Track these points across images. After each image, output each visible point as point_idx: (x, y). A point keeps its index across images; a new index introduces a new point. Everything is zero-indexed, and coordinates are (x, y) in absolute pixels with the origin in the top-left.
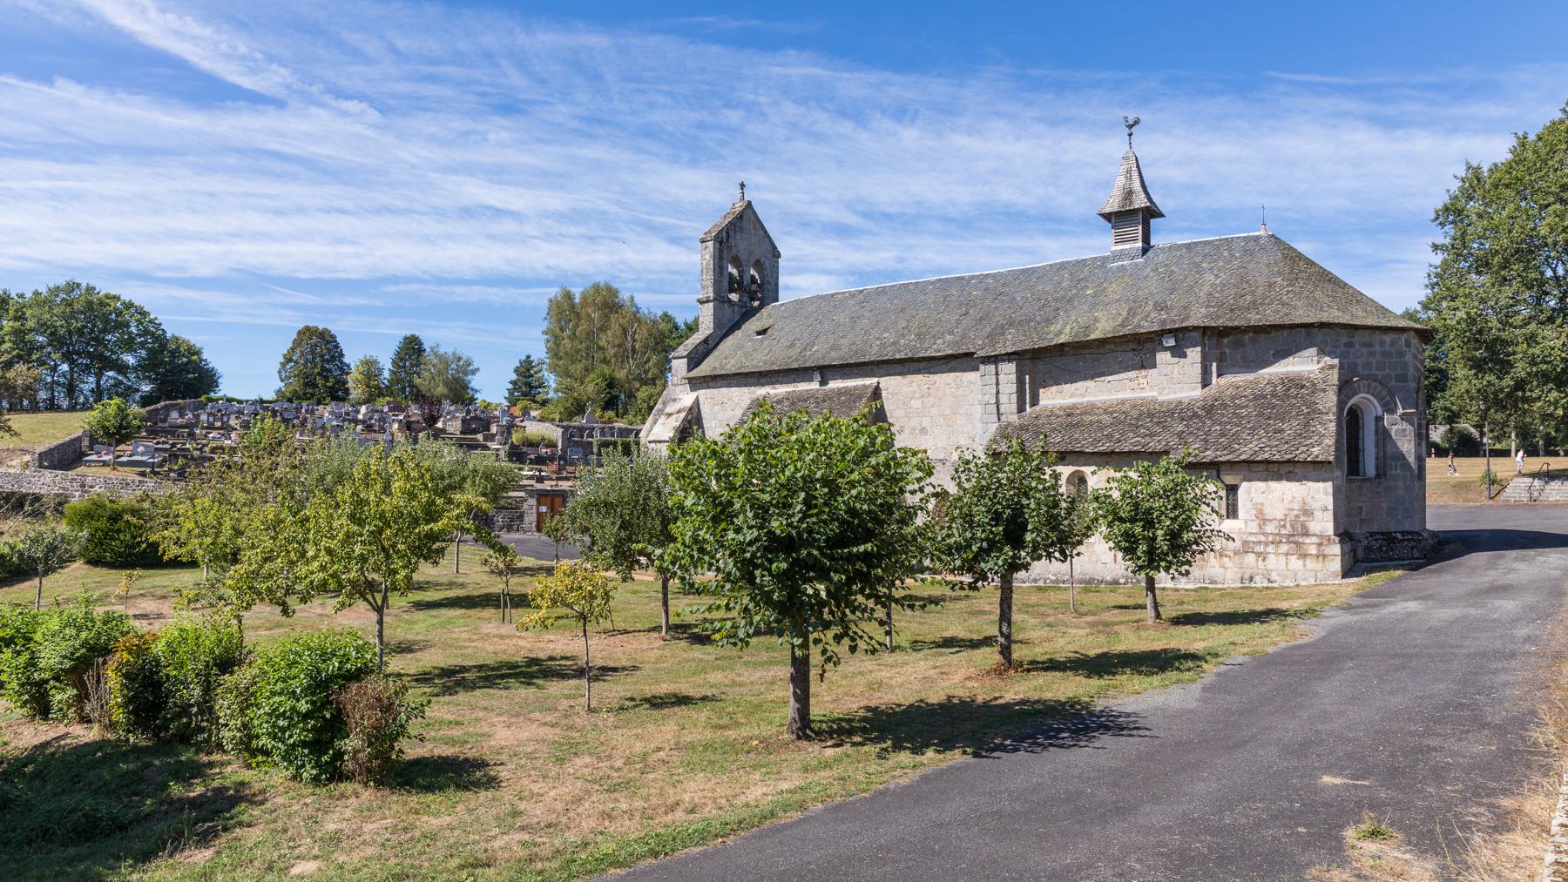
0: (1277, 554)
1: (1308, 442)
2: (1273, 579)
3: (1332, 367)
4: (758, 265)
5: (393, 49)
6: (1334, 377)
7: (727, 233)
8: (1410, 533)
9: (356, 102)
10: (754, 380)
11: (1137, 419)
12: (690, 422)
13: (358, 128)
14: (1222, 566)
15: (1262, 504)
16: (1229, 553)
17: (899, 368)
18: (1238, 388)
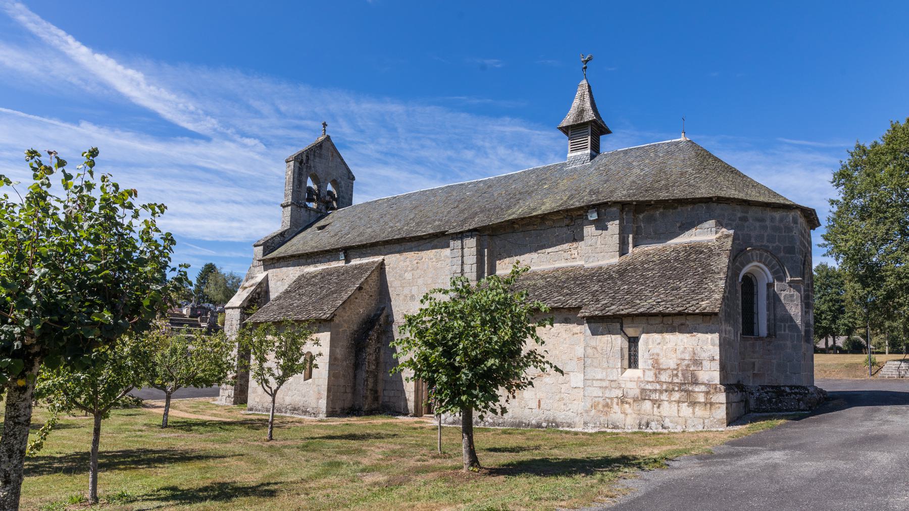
0: (670, 402)
1: (700, 297)
2: (666, 425)
3: (727, 236)
4: (335, 183)
5: (278, 111)
6: (729, 244)
7: (307, 156)
8: (797, 387)
9: (253, 139)
10: (303, 261)
11: (564, 282)
12: (259, 294)
13: (252, 154)
14: (624, 413)
15: (658, 355)
16: (629, 400)
17: (397, 247)
18: (648, 255)
